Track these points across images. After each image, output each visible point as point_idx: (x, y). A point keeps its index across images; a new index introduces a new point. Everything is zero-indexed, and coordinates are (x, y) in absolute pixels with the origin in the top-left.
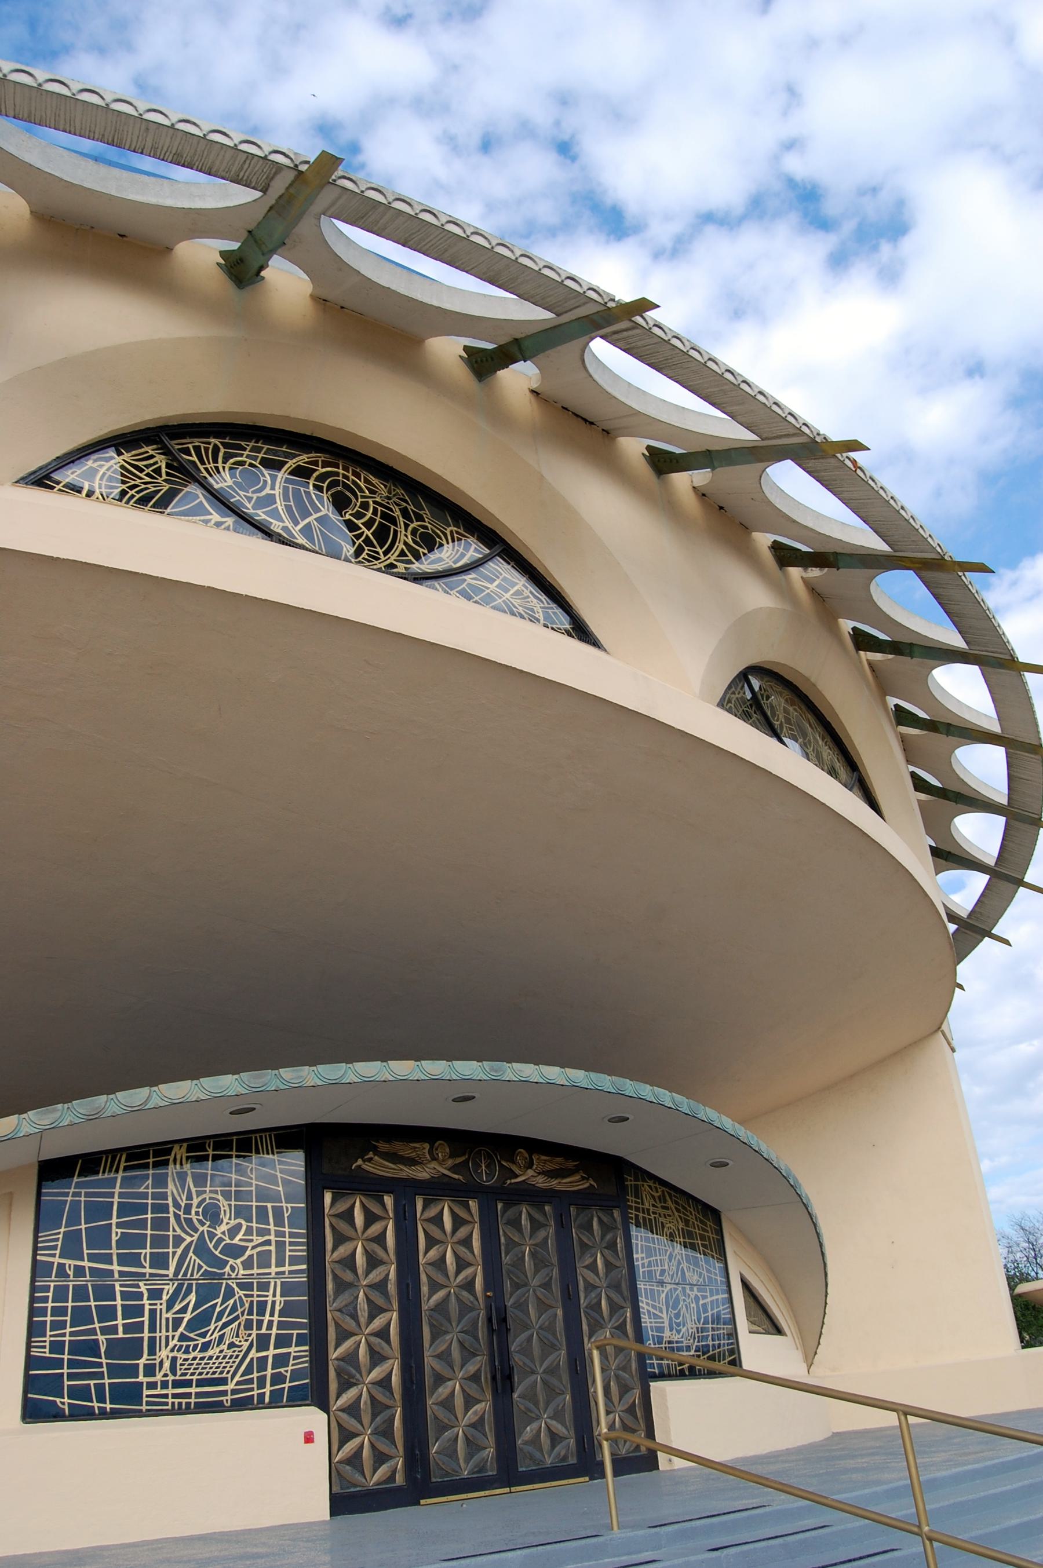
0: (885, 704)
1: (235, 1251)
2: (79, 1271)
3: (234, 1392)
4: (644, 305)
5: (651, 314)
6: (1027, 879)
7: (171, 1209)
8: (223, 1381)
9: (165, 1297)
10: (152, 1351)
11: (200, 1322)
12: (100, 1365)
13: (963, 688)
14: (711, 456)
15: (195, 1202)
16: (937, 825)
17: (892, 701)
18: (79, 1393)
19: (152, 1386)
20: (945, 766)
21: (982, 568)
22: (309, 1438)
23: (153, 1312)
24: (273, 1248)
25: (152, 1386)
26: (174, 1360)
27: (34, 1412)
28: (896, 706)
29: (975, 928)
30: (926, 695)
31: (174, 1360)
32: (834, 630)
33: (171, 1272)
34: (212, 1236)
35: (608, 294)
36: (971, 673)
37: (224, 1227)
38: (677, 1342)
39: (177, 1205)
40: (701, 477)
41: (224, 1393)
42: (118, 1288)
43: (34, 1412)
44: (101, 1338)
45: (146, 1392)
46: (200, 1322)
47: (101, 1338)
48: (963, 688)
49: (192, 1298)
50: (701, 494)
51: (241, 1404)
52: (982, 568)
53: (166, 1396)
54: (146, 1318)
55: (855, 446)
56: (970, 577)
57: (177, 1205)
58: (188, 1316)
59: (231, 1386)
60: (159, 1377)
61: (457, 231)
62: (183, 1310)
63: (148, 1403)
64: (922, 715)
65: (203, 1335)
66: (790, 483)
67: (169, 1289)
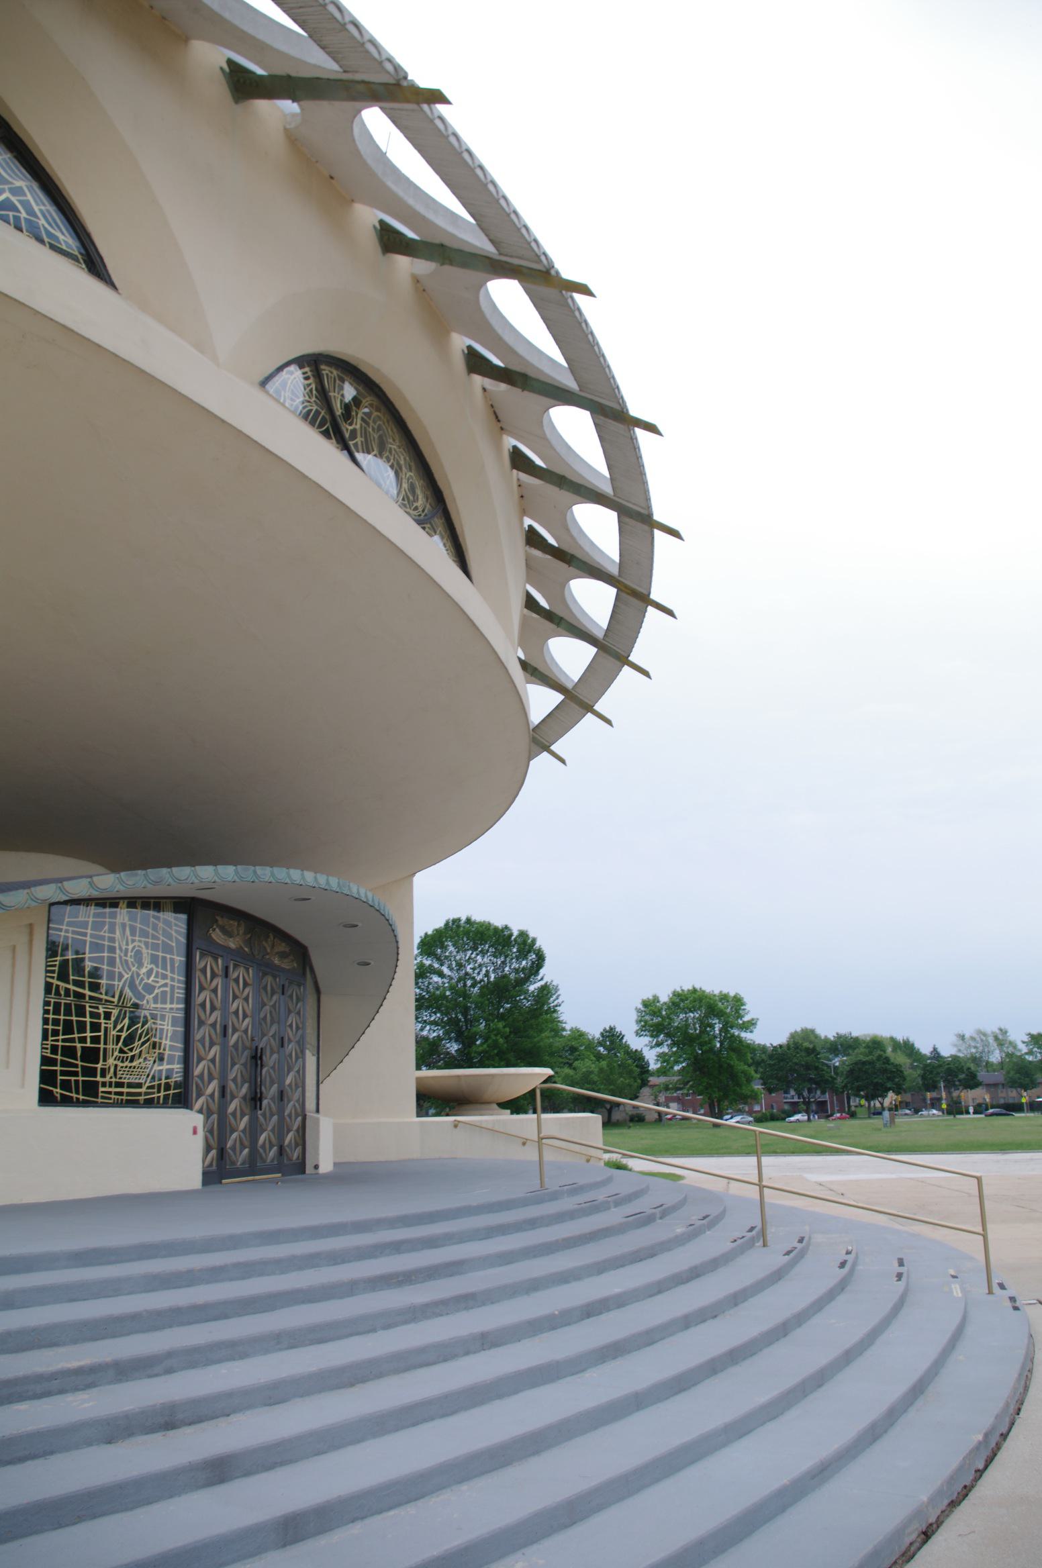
0: (522, 523)
1: (149, 989)
2: (67, 991)
3: (146, 1094)
4: (437, 97)
5: (441, 108)
6: (598, 707)
7: (118, 951)
8: (139, 1085)
9: (113, 1019)
10: (105, 1060)
11: (130, 1040)
12: (76, 1066)
13: (598, 527)
14: (441, 251)
15: (130, 947)
16: (532, 640)
17: (528, 521)
18: (66, 1085)
19: (104, 1084)
20: (559, 591)
21: (651, 428)
22: (195, 1132)
23: (106, 1029)
24: (168, 989)
25: (104, 1084)
26: (116, 1066)
27: (46, 1098)
28: (530, 527)
29: (541, 739)
30: (564, 524)
31: (116, 1066)
32: (498, 445)
33: (116, 1000)
34: (138, 975)
35: (350, 14)
36: (611, 516)
37: (144, 970)
38: (130, 1085)
39: (121, 949)
40: (423, 267)
41: (139, 1094)
42: (88, 1009)
43: (46, 1098)
44: (79, 1045)
45: (101, 1089)
46: (130, 1040)
47: (79, 1045)
48: (598, 527)
49: (126, 1021)
50: (416, 280)
51: (149, 1103)
52: (651, 428)
53: (110, 1093)
54: (102, 1033)
55: (585, 290)
56: (640, 433)
57: (121, 949)
58: (124, 1035)
59: (143, 1090)
60: (107, 1079)
61: (337, 15)
62: (121, 1030)
63: (103, 1098)
64: (551, 540)
65: (131, 1050)
66: (508, 298)
67: (115, 1012)
